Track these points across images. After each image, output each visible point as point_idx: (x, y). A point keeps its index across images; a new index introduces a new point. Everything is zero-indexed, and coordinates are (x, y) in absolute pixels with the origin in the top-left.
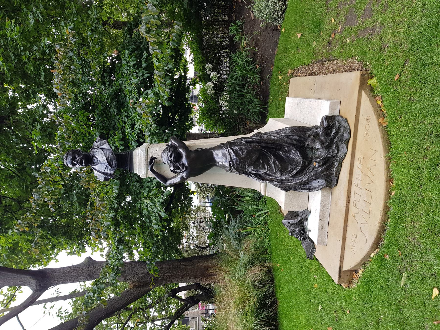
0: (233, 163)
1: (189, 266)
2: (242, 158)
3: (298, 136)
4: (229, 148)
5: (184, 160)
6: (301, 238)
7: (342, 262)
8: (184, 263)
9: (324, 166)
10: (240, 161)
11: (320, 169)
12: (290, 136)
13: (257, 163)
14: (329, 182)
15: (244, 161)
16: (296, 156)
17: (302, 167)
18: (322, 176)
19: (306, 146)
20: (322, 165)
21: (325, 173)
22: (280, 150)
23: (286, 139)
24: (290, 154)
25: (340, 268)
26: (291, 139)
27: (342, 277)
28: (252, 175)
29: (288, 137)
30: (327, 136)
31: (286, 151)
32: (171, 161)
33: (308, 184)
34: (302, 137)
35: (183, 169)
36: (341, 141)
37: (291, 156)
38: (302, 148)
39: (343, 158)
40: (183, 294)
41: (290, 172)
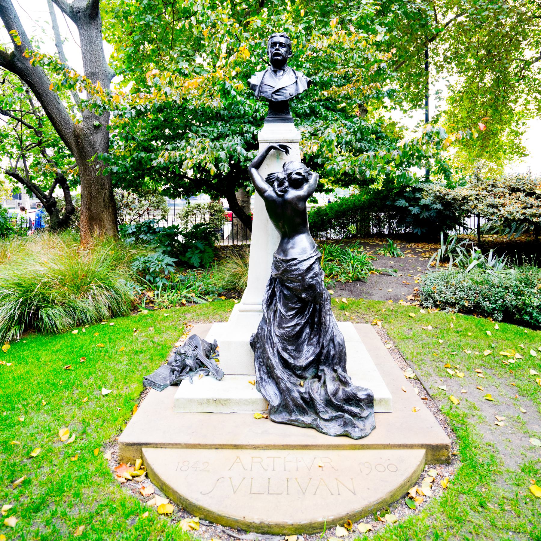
0: (295, 265)
1: (104, 201)
2: (303, 279)
3: (334, 355)
4: (316, 257)
5: (292, 194)
6: (176, 366)
7: (155, 445)
8: (107, 193)
9: (301, 402)
10: (300, 275)
11: (296, 395)
12: (333, 342)
13: (296, 300)
14: (277, 410)
15: (299, 281)
16: (308, 353)
17: (295, 366)
18: (286, 400)
19: (321, 367)
20: (303, 398)
21: (291, 403)
22: (312, 330)
23: (329, 338)
24: (307, 345)
25: (146, 445)
26: (329, 345)
27: (130, 448)
28: (270, 291)
29: (332, 340)
30: (345, 400)
31: (310, 339)
32: (291, 174)
33: (269, 377)
34: (333, 360)
35: (281, 191)
36: (345, 424)
37: (305, 347)
38: (318, 362)
39: (317, 429)
40: (58, 193)
41: (285, 350)
